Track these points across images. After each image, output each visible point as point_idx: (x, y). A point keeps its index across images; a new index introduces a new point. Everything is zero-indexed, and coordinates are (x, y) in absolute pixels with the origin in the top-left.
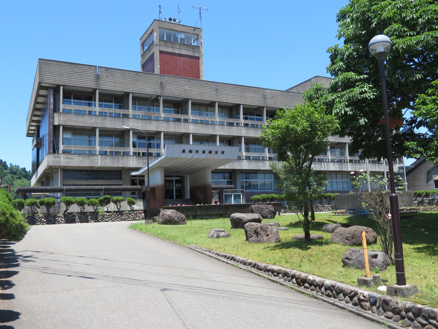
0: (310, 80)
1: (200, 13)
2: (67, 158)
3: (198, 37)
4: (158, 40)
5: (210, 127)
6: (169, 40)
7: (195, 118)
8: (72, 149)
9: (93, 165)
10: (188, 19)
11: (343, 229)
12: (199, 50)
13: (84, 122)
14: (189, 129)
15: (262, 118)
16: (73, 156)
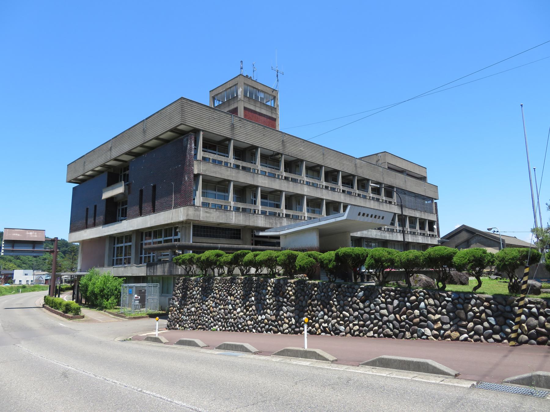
0: (376, 154)
1: (277, 76)
2: (206, 212)
3: (274, 98)
4: (243, 96)
5: (319, 190)
6: (250, 98)
7: (308, 180)
8: (211, 202)
9: (228, 222)
10: (266, 79)
11: (247, 345)
12: (276, 111)
13: (221, 174)
14: (304, 191)
15: (226, 194)
16: (212, 211)
